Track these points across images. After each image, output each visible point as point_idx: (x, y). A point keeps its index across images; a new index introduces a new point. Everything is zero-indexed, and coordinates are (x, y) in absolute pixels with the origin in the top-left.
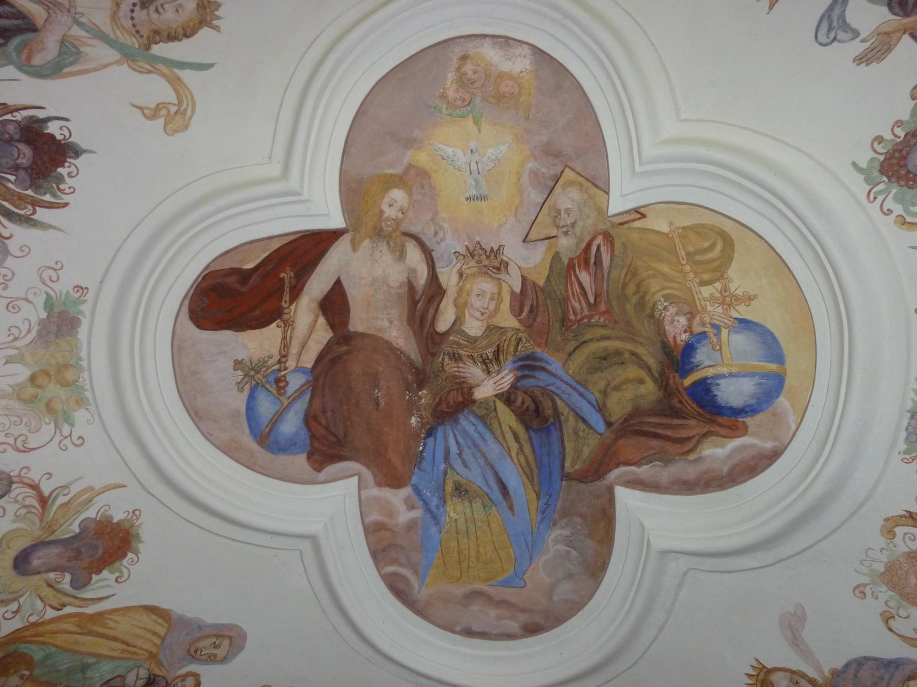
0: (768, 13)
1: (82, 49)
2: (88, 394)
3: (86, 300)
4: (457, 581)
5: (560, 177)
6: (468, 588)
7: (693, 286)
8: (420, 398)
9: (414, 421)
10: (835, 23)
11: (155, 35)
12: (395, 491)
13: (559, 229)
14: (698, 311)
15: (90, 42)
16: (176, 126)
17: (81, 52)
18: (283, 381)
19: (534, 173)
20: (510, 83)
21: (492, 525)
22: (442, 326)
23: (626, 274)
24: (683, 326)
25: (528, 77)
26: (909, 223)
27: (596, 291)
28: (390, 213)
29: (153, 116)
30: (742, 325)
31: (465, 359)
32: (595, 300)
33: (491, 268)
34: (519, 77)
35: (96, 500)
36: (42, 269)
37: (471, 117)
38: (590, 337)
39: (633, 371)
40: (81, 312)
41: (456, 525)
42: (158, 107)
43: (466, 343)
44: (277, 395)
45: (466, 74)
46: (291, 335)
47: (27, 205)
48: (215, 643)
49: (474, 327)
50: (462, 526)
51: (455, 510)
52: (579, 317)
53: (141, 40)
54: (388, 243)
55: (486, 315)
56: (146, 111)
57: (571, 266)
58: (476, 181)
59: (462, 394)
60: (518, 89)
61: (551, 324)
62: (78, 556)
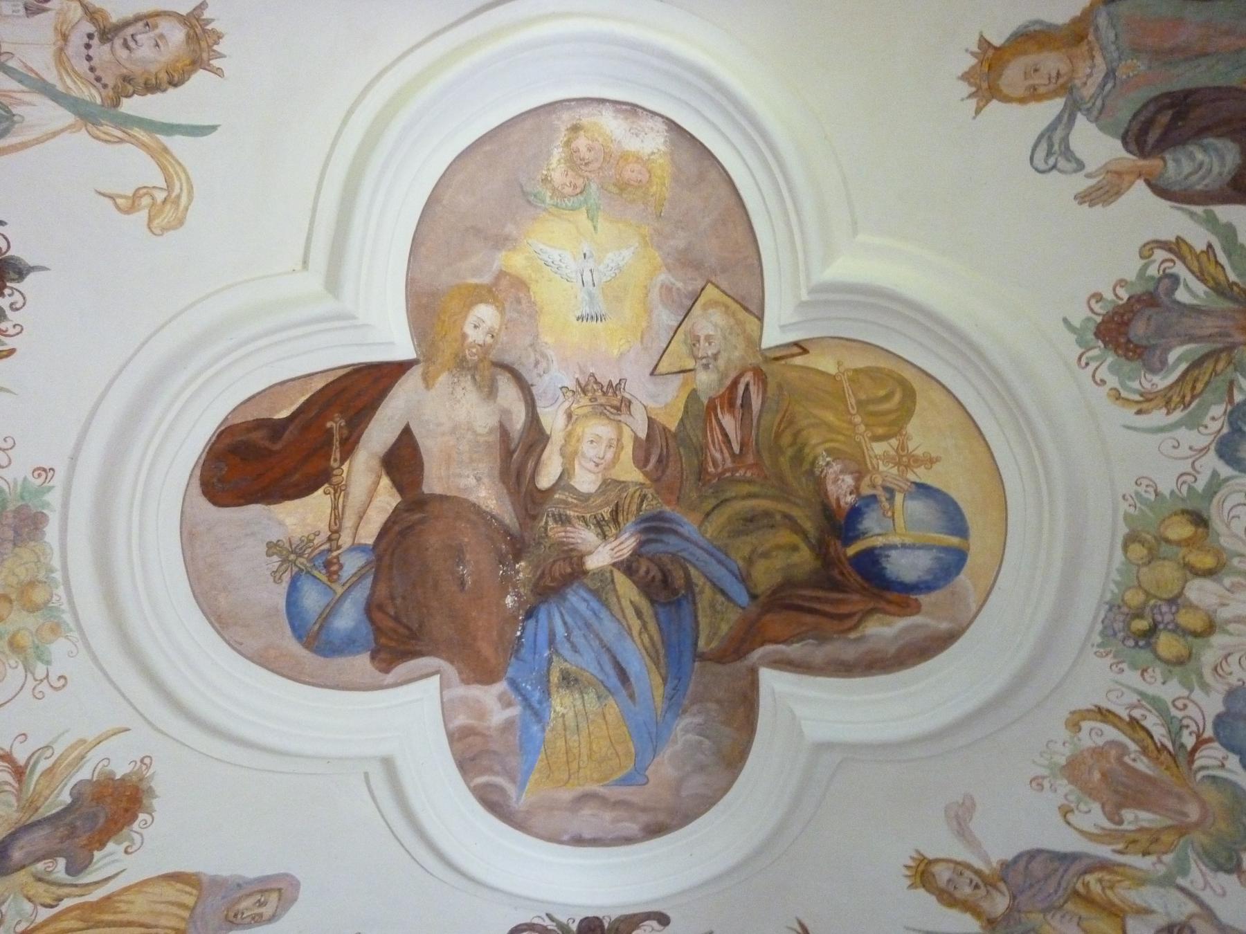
0: (974, 118)
1: (14, 111)
2: (67, 617)
3: (53, 487)
4: (565, 785)
5: (700, 295)
6: (579, 790)
7: (863, 441)
8: (518, 572)
9: (509, 601)
10: (1056, 147)
12: (486, 687)
13: (698, 361)
14: (868, 471)
15: (27, 97)
17: (14, 115)
18: (335, 564)
19: (667, 287)
20: (637, 167)
21: (608, 717)
22: (545, 480)
23: (781, 421)
24: (848, 487)
25: (661, 161)
26: (1123, 398)
27: (742, 438)
28: (475, 336)
29: (131, 208)
30: (921, 490)
31: (574, 521)
32: (741, 450)
33: (608, 408)
34: (649, 159)
35: (89, 755)
37: (584, 210)
38: (733, 494)
39: (785, 537)
40: (47, 505)
41: (564, 721)
42: (136, 196)
43: (575, 501)
44: (329, 583)
45: (578, 151)
48: (259, 901)
49: (586, 481)
50: (571, 722)
51: (562, 704)
52: (720, 470)
53: (104, 92)
54: (473, 377)
55: (601, 467)
56: (119, 201)
57: (711, 407)
58: (590, 294)
59: (571, 564)
60: (648, 175)
61: (685, 477)
62: (72, 832)
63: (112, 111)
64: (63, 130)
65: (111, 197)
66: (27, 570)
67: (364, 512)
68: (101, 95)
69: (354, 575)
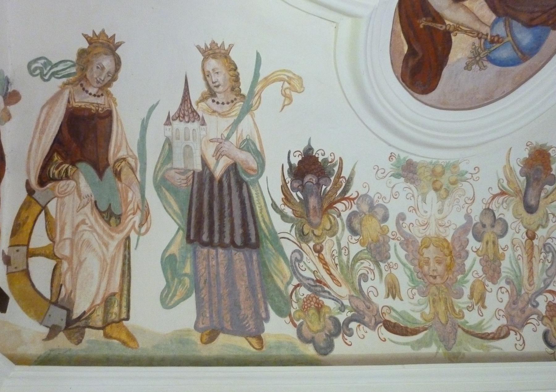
1: (245, 138)
11: (235, 90)
15: (239, 132)
16: (298, 85)
17: (247, 138)
35: (512, 165)
36: (378, 178)
40: (405, 158)
42: (285, 95)
44: (502, 44)
46: (466, 27)
47: (340, 181)
53: (238, 100)
56: (286, 103)
62: (537, 180)
63: (247, 99)
64: (253, 120)
65: (284, 106)
66: (427, 171)
67: (477, 17)
68: (239, 102)
69: (506, 29)
